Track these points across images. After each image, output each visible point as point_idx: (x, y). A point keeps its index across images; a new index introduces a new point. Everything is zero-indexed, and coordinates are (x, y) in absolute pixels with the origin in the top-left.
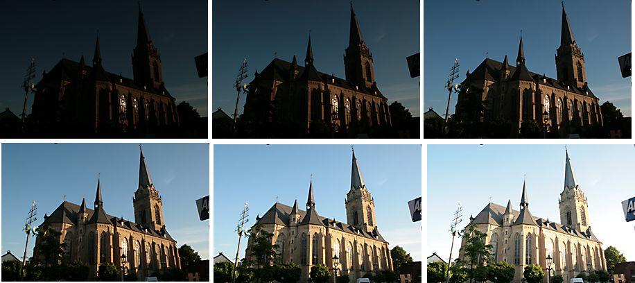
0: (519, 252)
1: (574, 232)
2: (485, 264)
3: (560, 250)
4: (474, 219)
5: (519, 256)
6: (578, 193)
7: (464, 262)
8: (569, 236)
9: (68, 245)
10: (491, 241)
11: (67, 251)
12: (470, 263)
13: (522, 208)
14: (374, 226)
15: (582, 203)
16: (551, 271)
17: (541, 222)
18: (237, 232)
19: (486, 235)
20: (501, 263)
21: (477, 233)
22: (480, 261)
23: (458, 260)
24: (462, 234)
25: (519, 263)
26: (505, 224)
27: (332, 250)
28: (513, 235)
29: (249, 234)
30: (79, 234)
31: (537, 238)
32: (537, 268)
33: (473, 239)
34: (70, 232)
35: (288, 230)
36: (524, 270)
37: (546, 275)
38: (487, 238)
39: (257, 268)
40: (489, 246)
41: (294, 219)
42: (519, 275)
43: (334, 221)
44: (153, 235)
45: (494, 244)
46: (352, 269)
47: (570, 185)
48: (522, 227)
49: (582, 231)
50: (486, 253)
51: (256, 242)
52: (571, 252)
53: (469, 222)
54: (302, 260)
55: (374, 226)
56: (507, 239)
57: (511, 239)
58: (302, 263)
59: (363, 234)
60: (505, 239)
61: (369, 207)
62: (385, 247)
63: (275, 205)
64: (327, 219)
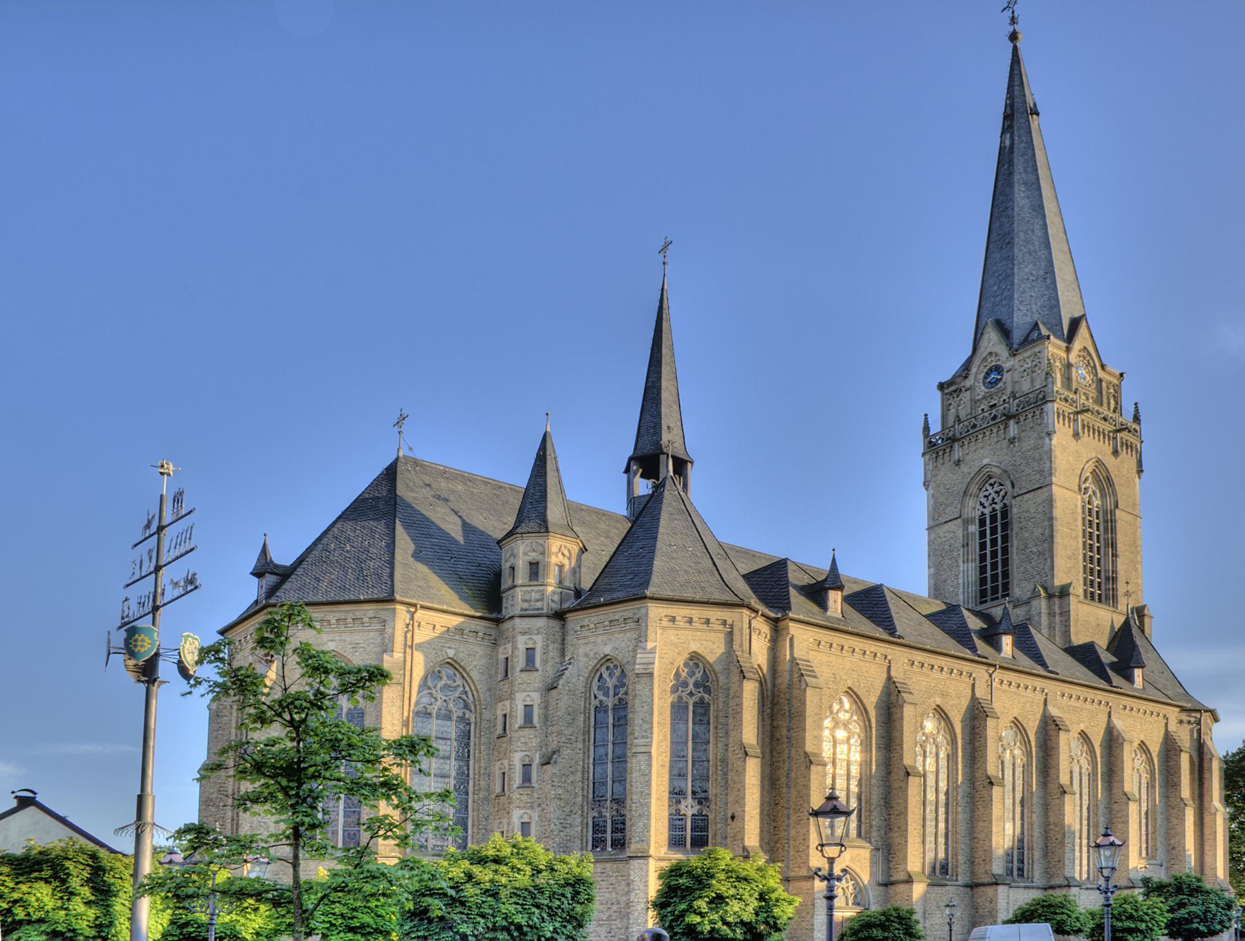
0: (621, 779)
1: (1025, 644)
2: (387, 854)
3: (911, 756)
4: (284, 574)
5: (619, 801)
6: (1081, 374)
7: (242, 846)
8: (981, 672)
9: (443, 747)
10: (424, 714)
11: (432, 785)
12: (286, 851)
13: (643, 487)
14: (1124, 604)
15: (1103, 449)
16: (843, 889)
17: (783, 583)
18: (118, 660)
19: (377, 675)
20: (496, 843)
21: (316, 666)
22: (351, 837)
23: (198, 835)
24: (210, 672)
25: (619, 844)
26: (518, 598)
27: (809, 761)
28: (577, 675)
29: (210, 672)
30: (518, 676)
31: (750, 691)
32: (748, 869)
33: (287, 704)
34: (453, 664)
35: (495, 644)
36: (653, 887)
37: (806, 910)
38: (389, 694)
39: (286, 880)
40: (410, 747)
41: (535, 569)
42: (625, 912)
43: (833, 580)
44: (1053, 676)
45: (442, 731)
46: (941, 872)
47: (1020, 320)
48: (639, 622)
49: (1078, 639)
50: (389, 787)
51: (262, 719)
52: (992, 769)
53: (249, 591)
54: (598, 828)
55: (1124, 604)
56: (536, 698)
57: (563, 701)
58: (598, 843)
59: (1038, 658)
60: (520, 700)
61: (1104, 480)
62: (1184, 737)
63: (390, 473)
64: (781, 565)
